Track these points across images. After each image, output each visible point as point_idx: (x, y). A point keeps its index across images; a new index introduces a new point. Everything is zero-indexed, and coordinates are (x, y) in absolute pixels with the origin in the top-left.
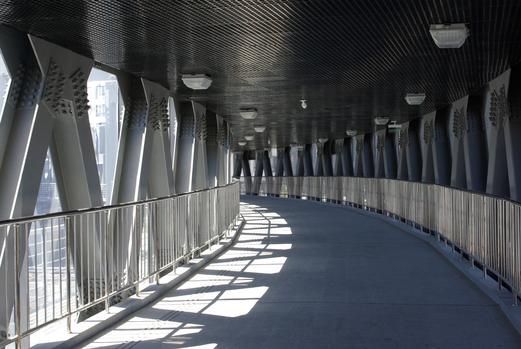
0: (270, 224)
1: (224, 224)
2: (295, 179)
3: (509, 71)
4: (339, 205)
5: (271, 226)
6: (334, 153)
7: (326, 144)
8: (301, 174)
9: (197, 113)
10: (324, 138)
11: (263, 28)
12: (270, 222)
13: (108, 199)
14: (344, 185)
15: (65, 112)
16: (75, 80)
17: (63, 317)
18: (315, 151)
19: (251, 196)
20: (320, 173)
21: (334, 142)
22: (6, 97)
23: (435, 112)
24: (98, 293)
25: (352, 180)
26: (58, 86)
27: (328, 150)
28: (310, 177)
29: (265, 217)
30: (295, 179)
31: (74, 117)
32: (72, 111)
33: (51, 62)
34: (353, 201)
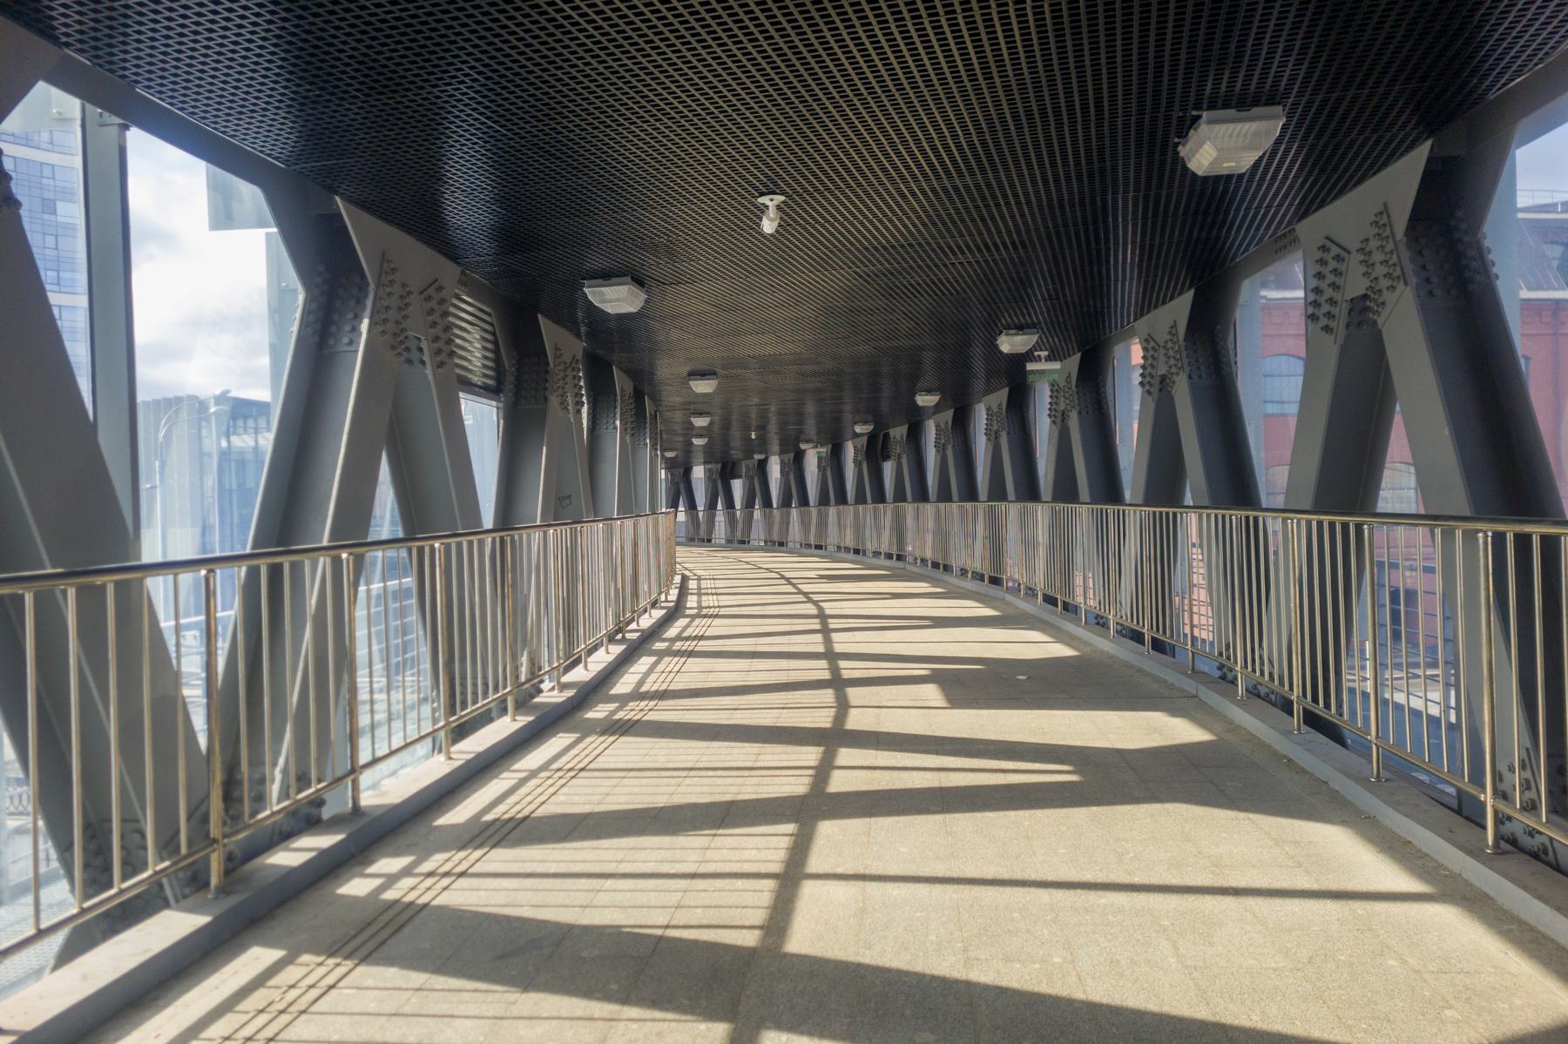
0: (822, 616)
1: (664, 585)
2: (1135, 517)
3: (1191, 293)
4: (900, 564)
5: (833, 623)
6: (886, 457)
7: (872, 437)
8: (824, 501)
9: (622, 390)
10: (865, 423)
11: (828, 131)
12: (821, 609)
13: (488, 521)
14: (910, 521)
15: (409, 361)
16: (429, 298)
17: (421, 738)
18: (850, 451)
19: (699, 536)
20: (945, 496)
21: (887, 436)
22: (295, 328)
23: (1007, 390)
24: (475, 693)
25: (929, 509)
26: (400, 309)
27: (876, 451)
28: (921, 505)
29: (805, 594)
30: (814, 511)
31: (429, 371)
32: (426, 358)
33: (384, 258)
34: (929, 554)
